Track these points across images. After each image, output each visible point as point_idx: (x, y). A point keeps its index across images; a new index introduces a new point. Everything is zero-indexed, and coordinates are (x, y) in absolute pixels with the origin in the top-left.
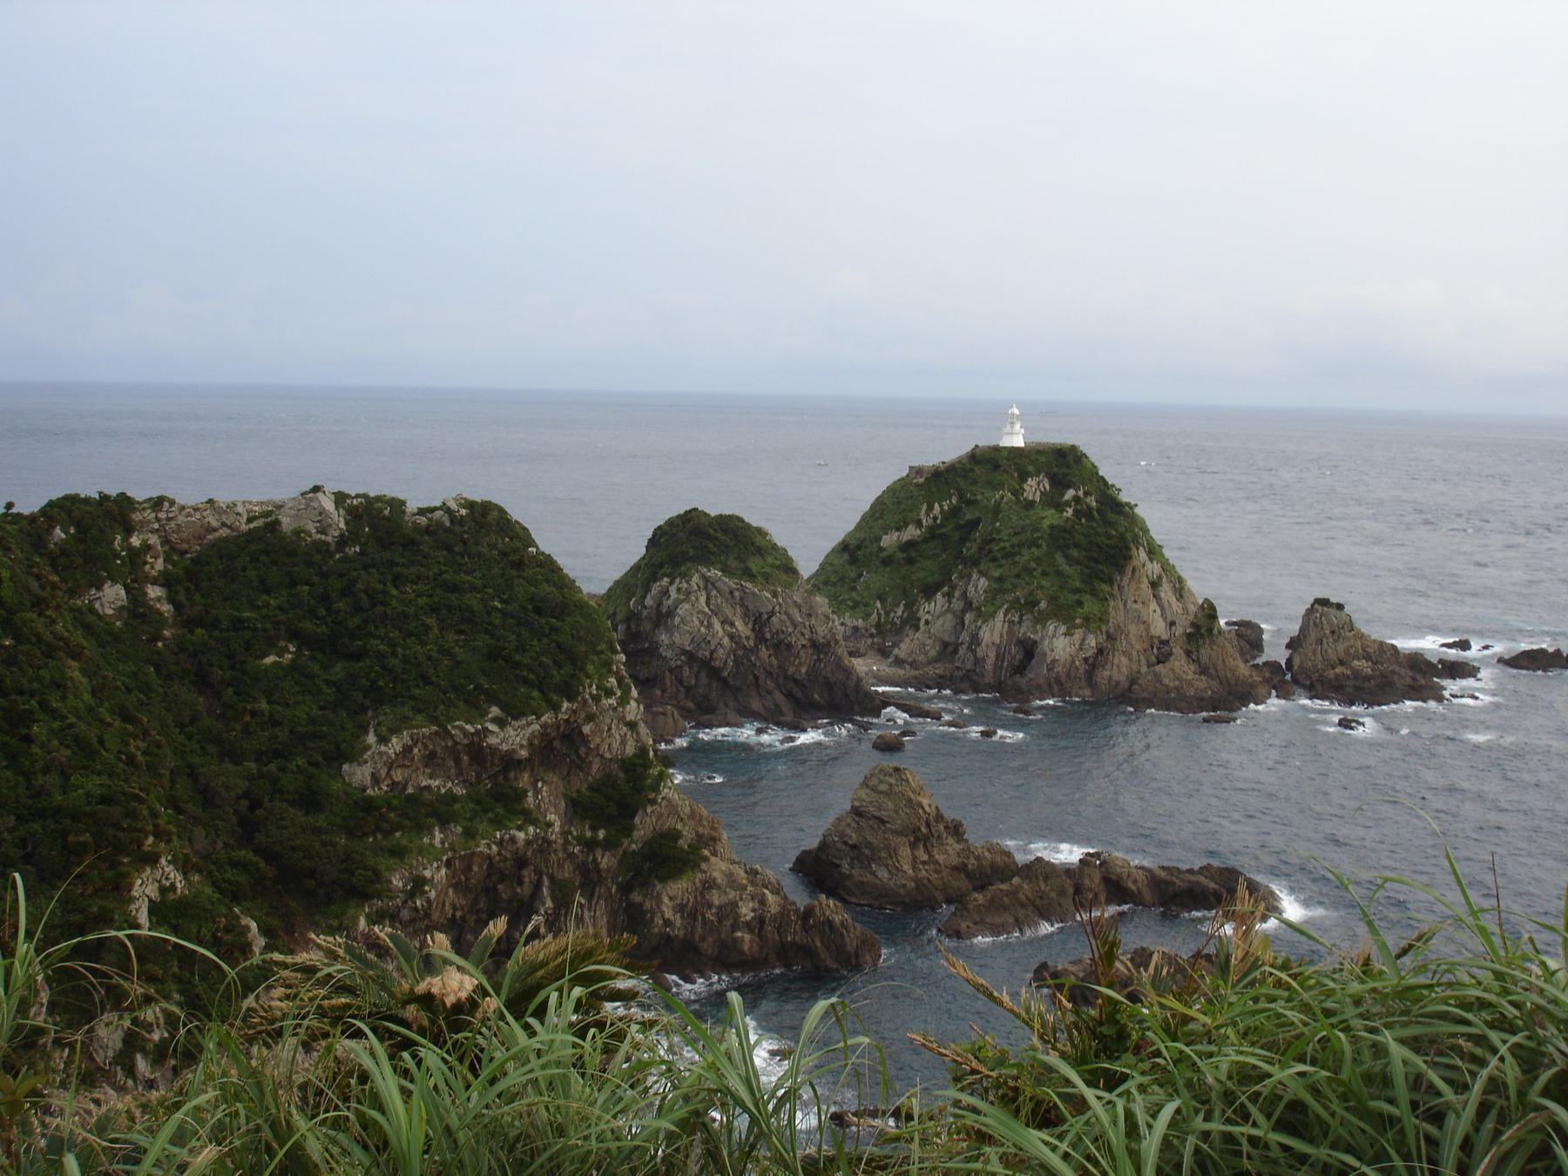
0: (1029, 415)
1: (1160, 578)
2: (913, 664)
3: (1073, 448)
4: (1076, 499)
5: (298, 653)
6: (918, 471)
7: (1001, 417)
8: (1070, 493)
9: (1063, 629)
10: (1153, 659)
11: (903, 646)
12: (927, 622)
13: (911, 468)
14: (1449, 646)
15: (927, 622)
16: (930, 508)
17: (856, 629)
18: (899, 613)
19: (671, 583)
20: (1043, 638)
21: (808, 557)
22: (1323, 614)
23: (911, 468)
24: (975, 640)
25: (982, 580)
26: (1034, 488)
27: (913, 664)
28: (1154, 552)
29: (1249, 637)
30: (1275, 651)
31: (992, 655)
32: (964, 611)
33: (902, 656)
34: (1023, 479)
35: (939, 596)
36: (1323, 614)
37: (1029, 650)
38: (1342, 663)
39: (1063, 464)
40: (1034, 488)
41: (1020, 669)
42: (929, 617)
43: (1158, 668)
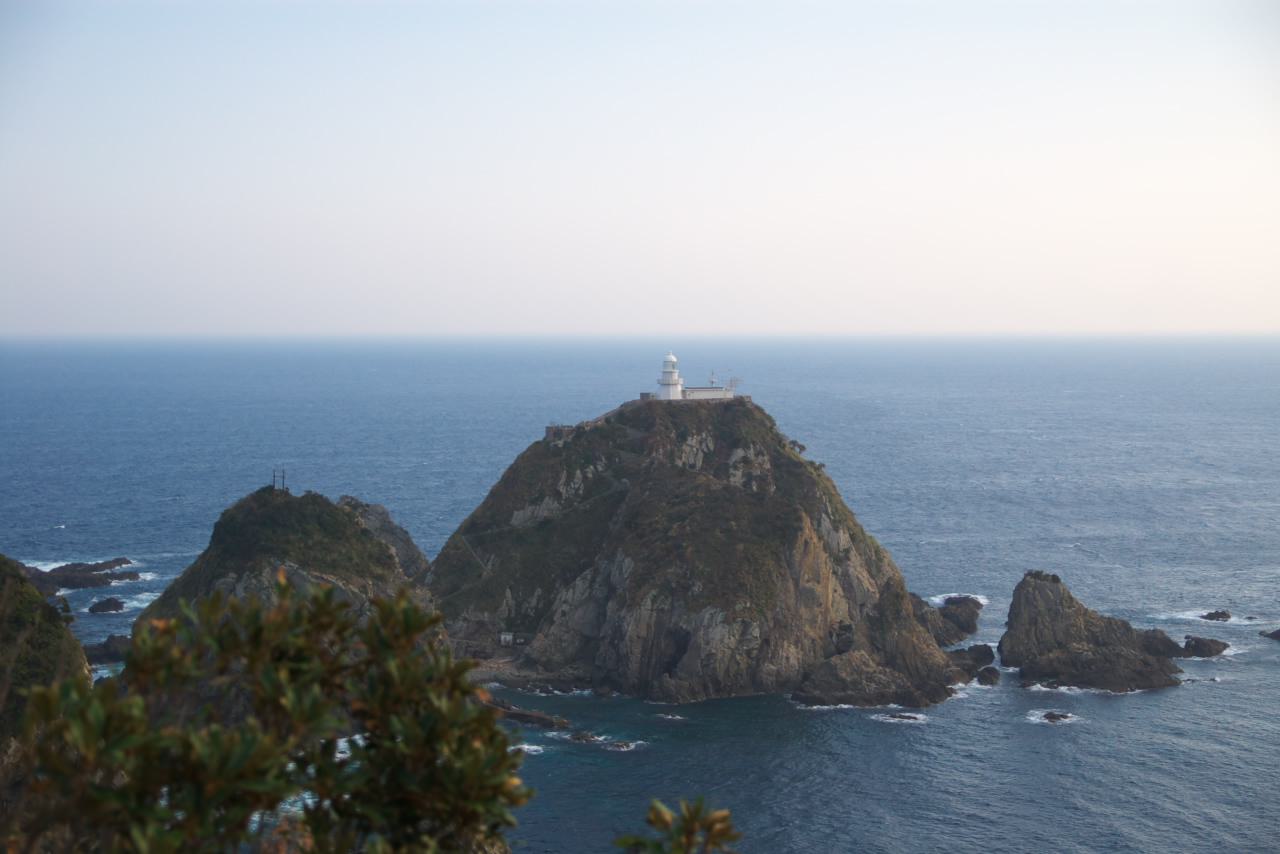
1: (847, 551)
2: (548, 666)
4: (745, 460)
7: (667, 369)
8: (740, 453)
9: (720, 617)
10: (833, 648)
11: (536, 644)
12: (564, 614)
14: (1203, 617)
16: (570, 477)
17: (481, 624)
19: (239, 580)
20: (696, 630)
21: (430, 544)
22: (1037, 595)
24: (619, 633)
25: (628, 561)
26: (694, 449)
27: (548, 666)
28: (843, 519)
29: (961, 615)
30: (990, 634)
31: (637, 650)
32: (607, 599)
33: (535, 655)
34: (682, 437)
35: (579, 582)
36: (1037, 595)
37: (682, 642)
38: (1060, 645)
39: (733, 421)
40: (694, 449)
41: (670, 667)
42: (565, 607)
43: (835, 660)
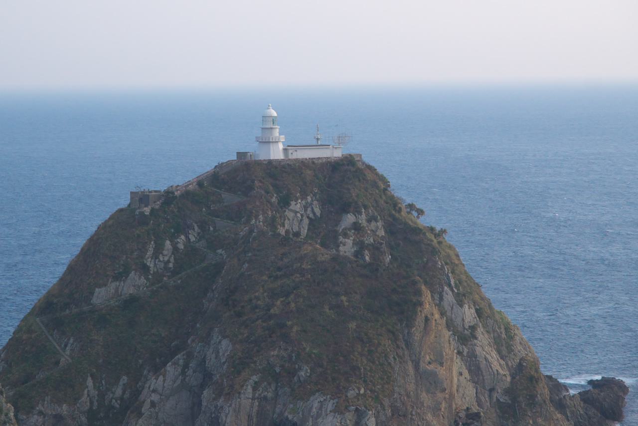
0: (341, 139)
1: (473, 328)
3: (349, 162)
4: (356, 227)
5: (365, 261)
6: (141, 198)
8: (349, 219)
12: (153, 404)
13: (133, 194)
15: (153, 404)
18: (119, 392)
23: (133, 194)
26: (297, 216)
28: (467, 291)
32: (202, 386)
34: (285, 202)
39: (342, 183)
40: (297, 216)
42: (155, 397)
